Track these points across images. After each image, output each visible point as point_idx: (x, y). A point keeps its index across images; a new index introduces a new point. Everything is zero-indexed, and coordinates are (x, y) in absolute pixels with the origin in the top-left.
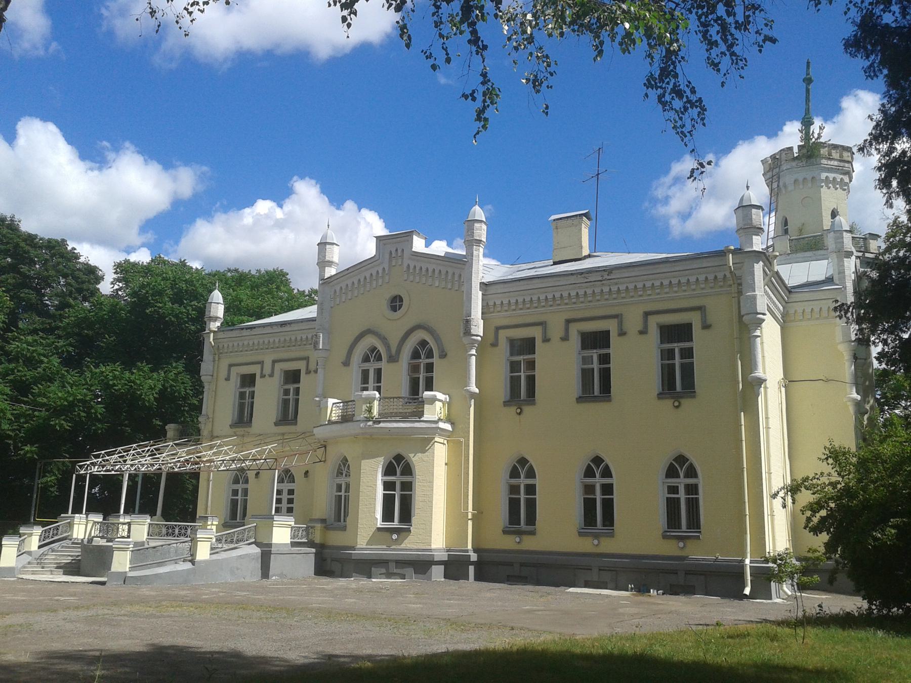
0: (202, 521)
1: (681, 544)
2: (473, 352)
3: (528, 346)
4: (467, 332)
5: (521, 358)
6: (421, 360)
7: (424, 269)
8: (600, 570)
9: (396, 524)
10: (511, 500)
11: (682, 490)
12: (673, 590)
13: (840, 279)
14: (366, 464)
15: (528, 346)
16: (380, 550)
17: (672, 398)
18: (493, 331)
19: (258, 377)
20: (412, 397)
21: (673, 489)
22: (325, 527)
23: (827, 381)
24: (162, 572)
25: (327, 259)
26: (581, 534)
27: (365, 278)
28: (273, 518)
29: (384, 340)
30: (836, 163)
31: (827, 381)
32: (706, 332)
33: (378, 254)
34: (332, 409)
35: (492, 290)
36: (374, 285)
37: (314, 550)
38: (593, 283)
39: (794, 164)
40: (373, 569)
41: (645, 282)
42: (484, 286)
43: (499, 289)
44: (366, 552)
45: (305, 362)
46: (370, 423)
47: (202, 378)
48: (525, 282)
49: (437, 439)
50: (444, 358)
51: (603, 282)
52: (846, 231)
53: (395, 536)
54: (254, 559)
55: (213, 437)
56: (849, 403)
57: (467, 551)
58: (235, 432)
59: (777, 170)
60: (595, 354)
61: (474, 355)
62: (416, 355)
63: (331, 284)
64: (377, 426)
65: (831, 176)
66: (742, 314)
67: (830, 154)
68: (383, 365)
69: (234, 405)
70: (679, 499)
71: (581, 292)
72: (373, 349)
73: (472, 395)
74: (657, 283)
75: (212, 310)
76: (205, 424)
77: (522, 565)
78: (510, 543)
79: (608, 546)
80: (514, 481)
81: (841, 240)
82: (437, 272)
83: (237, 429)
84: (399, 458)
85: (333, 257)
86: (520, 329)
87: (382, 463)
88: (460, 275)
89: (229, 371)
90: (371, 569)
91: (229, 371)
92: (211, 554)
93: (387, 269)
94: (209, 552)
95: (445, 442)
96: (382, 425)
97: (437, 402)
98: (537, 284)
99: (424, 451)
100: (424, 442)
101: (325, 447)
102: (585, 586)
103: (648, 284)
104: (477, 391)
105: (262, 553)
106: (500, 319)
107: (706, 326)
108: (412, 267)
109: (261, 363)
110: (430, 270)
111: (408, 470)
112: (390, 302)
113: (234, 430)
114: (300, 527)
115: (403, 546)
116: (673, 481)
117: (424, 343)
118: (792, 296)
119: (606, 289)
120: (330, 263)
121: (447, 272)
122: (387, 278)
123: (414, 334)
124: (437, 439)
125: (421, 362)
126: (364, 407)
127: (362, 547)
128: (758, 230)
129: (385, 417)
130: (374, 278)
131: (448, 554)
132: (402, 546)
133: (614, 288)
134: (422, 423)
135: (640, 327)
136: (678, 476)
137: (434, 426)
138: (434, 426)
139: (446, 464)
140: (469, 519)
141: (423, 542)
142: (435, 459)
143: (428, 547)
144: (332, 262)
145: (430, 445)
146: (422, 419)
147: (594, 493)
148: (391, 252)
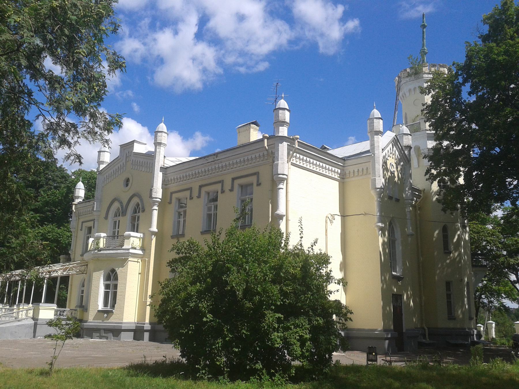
6: (136, 214)
9: (108, 308)
16: (98, 323)
19: (92, 228)
22: (82, 310)
23: (366, 214)
31: (366, 214)
34: (92, 244)
36: (119, 173)
38: (211, 163)
39: (408, 79)
40: (93, 333)
42: (164, 169)
44: (91, 324)
46: (96, 251)
49: (129, 259)
51: (215, 162)
53: (105, 315)
54: (28, 327)
56: (376, 228)
73: (153, 233)
85: (104, 159)
86: (180, 193)
87: (103, 274)
89: (82, 225)
91: (82, 225)
93: (124, 163)
95: (140, 261)
97: (131, 238)
99: (123, 267)
100: (123, 261)
101: (87, 265)
106: (173, 187)
112: (126, 182)
115: (109, 321)
118: (346, 162)
120: (103, 162)
122: (124, 168)
124: (129, 259)
125: (136, 215)
128: (283, 123)
132: (109, 320)
134: (121, 250)
137: (127, 251)
138: (127, 251)
139: (139, 274)
140: (148, 305)
141: (119, 318)
142: (128, 271)
143: (121, 322)
144: (104, 162)
146: (122, 248)
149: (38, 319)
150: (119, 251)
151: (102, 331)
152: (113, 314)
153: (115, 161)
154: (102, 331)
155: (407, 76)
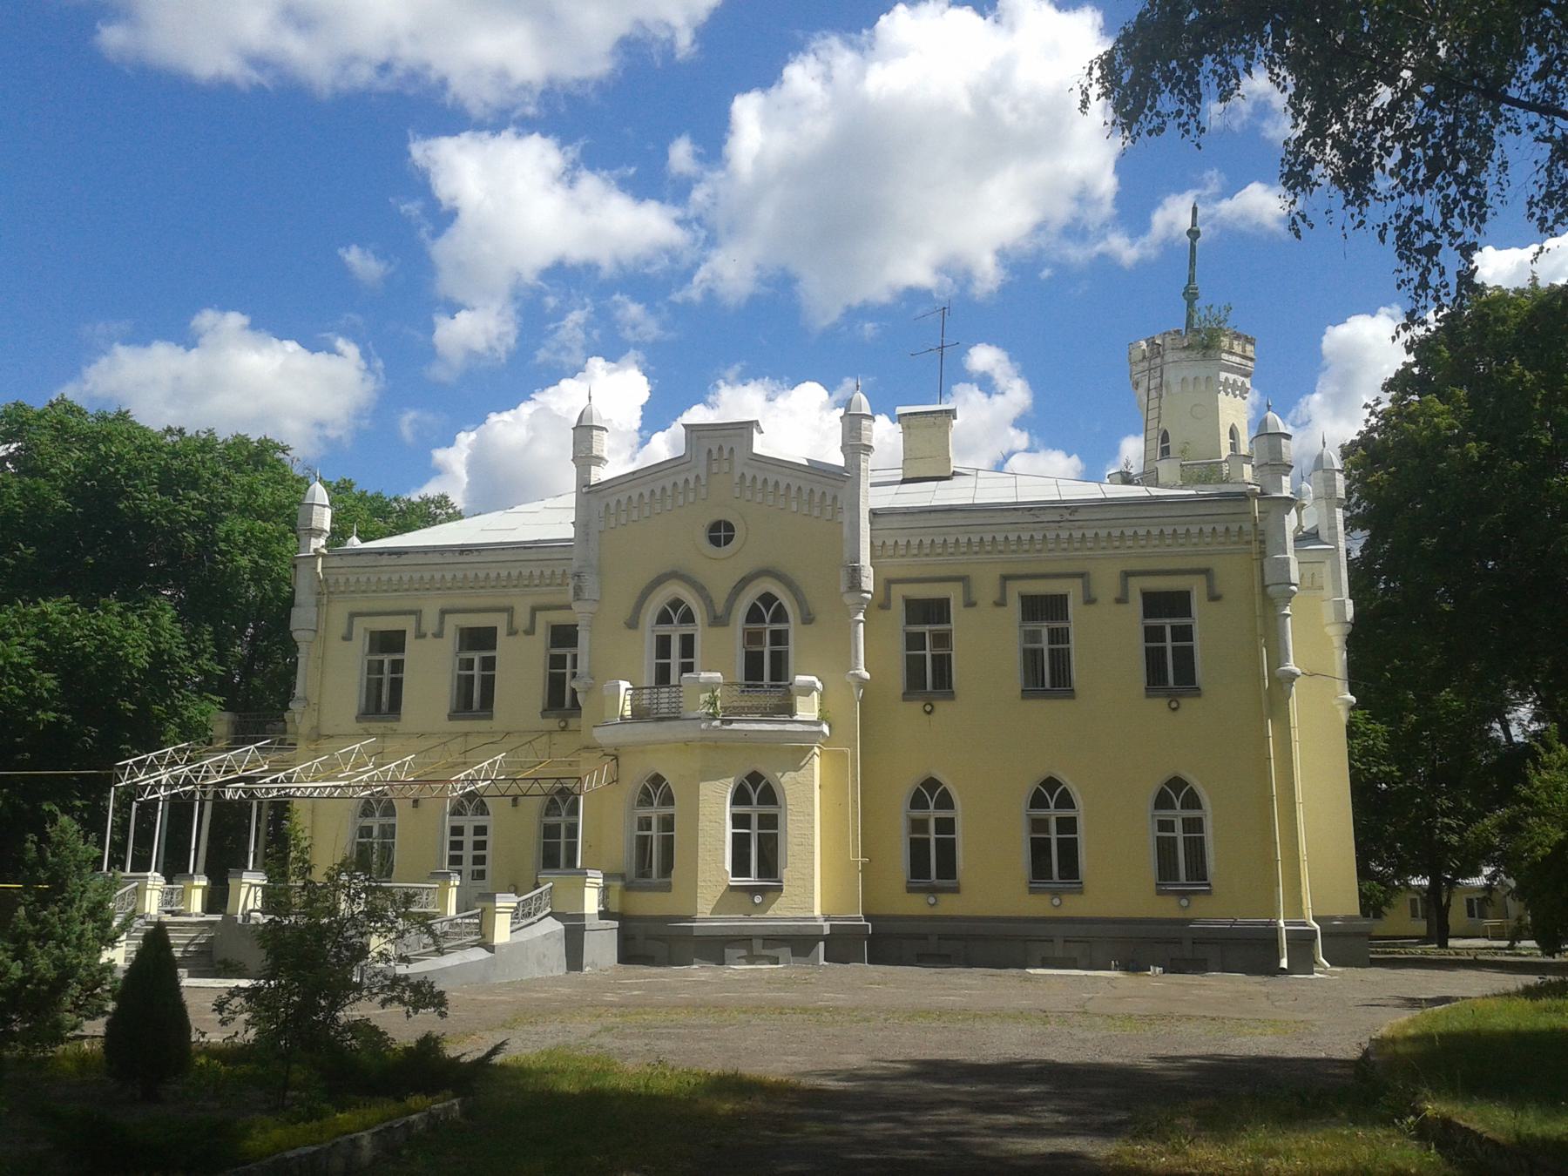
0: (439, 881)
1: (1184, 902)
2: (861, 616)
3: (934, 611)
4: (855, 585)
5: (926, 628)
7: (771, 483)
8: (1065, 941)
9: (752, 880)
10: (913, 842)
11: (1179, 825)
12: (1175, 966)
13: (1329, 537)
14: (706, 789)
15: (934, 611)
16: (735, 921)
17: (1168, 696)
18: (886, 584)
20: (774, 683)
21: (1165, 825)
24: (448, 965)
25: (595, 452)
26: (1032, 891)
27: (664, 489)
28: (586, 874)
29: (700, 590)
30: (1238, 360)
32: (971, 610)
33: (689, 454)
35: (882, 522)
36: (681, 502)
37: (616, 924)
39: (1183, 355)
41: (1136, 529)
42: (874, 513)
43: (896, 522)
45: (505, 616)
47: (295, 635)
48: (940, 515)
50: (810, 623)
51: (1061, 524)
52: (1338, 470)
53: (758, 899)
55: (317, 736)
57: (814, 919)
58: (365, 730)
59: (1158, 360)
60: (1044, 628)
61: (861, 621)
62: (754, 615)
63: (601, 494)
64: (727, 727)
65: (1232, 377)
66: (1267, 583)
67: (1231, 346)
68: (699, 630)
69: (452, 686)
70: (1175, 839)
71: (1025, 536)
72: (676, 604)
74: (1142, 532)
75: (314, 517)
76: (303, 713)
77: (943, 937)
78: (917, 905)
79: (1074, 906)
80: (918, 814)
81: (1332, 483)
82: (794, 489)
83: (374, 724)
84: (755, 778)
88: (835, 498)
90: (724, 952)
92: (512, 932)
94: (509, 929)
96: (735, 726)
98: (958, 519)
99: (797, 768)
101: (616, 758)
102: (1043, 966)
103: (1129, 532)
104: (867, 675)
105: (566, 930)
106: (897, 569)
107: (1214, 597)
108: (749, 478)
109: (417, 613)
110: (782, 486)
111: (769, 796)
113: (366, 725)
114: (423, 888)
115: (770, 913)
116: (1166, 814)
117: (768, 599)
119: (1064, 535)
121: (812, 490)
123: (755, 583)
126: (705, 697)
127: (705, 916)
129: (735, 714)
130: (669, 493)
131: (831, 925)
132: (769, 912)
133: (1077, 534)
134: (797, 725)
135: (1115, 592)
136: (1173, 807)
137: (815, 729)
138: (815, 729)
143: (810, 915)
145: (807, 758)
146: (795, 718)
147: (1047, 830)
148: (710, 451)
149: (584, 915)
150: (789, 727)
151: (757, 944)
152: (779, 896)
153: (665, 466)
154: (757, 944)
155: (1184, 348)
